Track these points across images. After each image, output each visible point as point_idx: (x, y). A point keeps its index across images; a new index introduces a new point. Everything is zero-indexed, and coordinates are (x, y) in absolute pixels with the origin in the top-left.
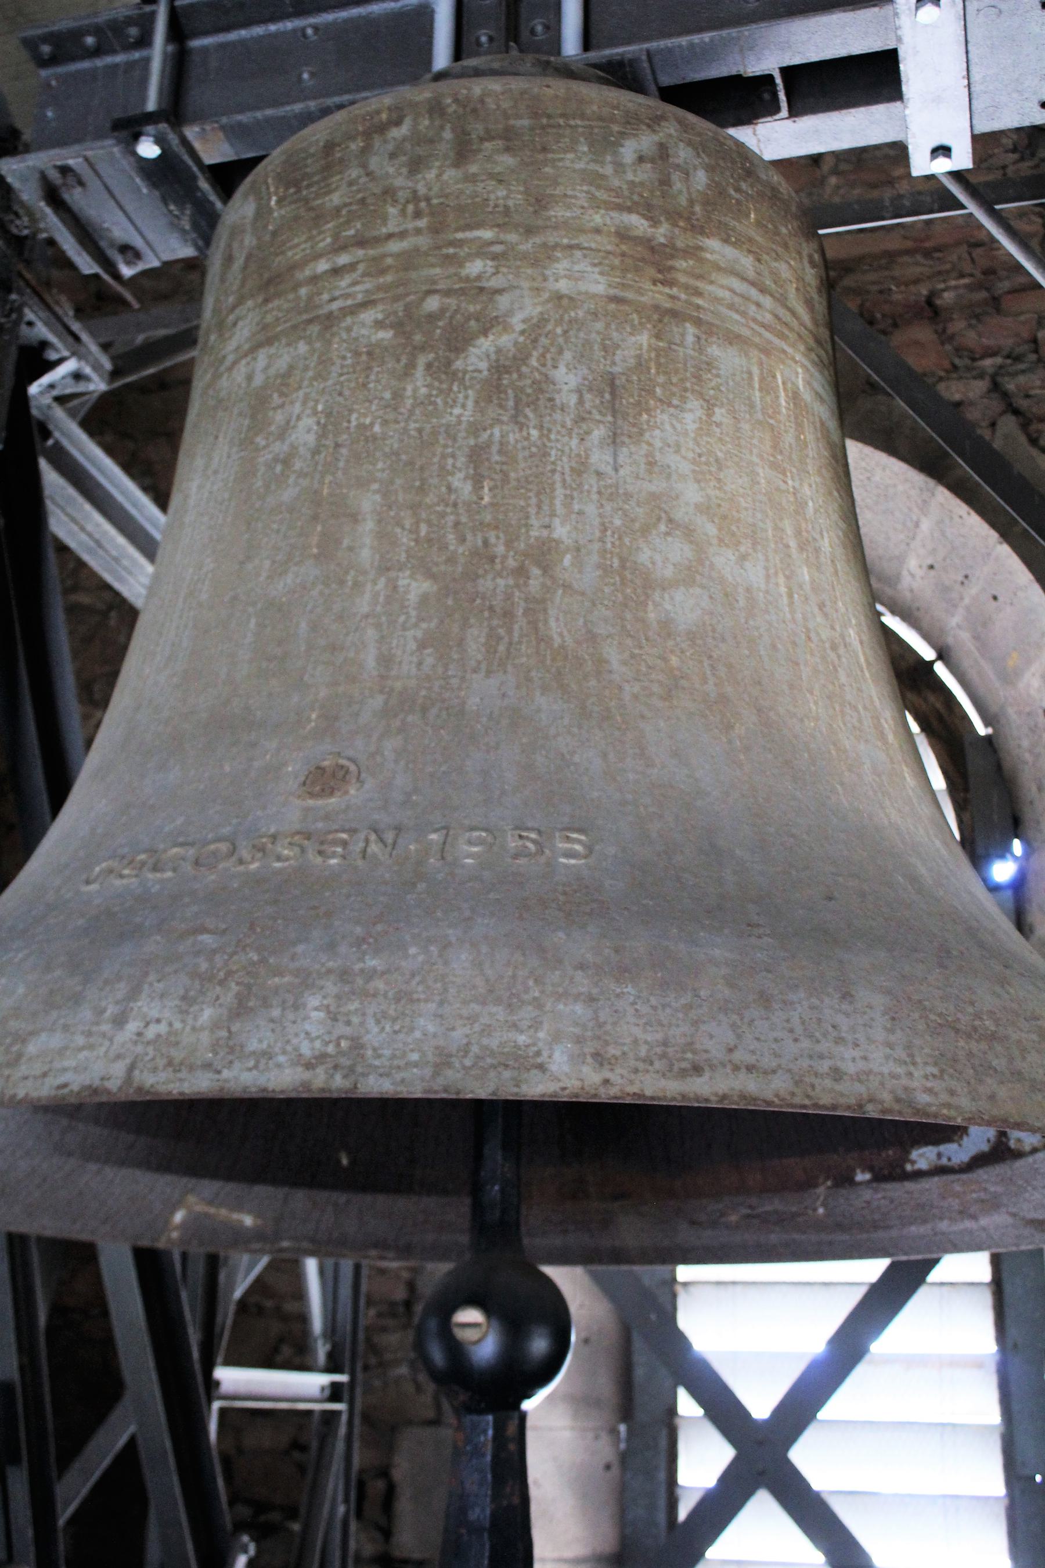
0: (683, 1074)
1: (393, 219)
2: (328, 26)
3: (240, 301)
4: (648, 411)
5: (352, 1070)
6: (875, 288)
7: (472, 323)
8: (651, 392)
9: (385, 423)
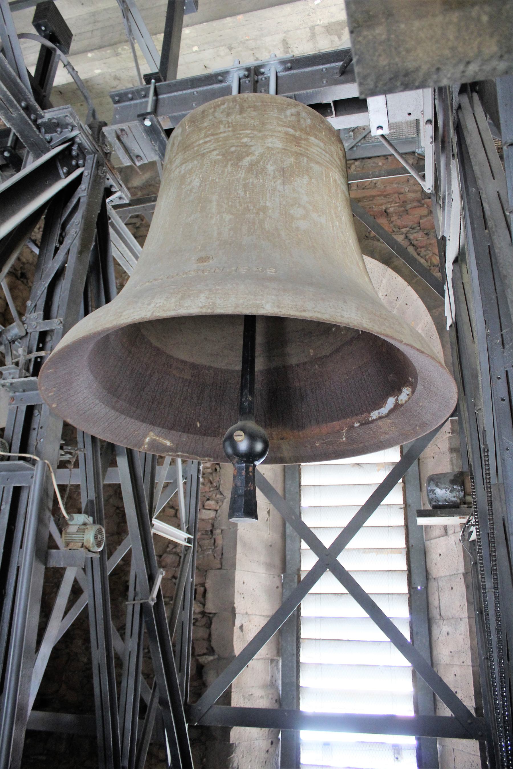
0: (301, 311)
1: (222, 128)
2: (201, 91)
3: (177, 154)
4: (293, 177)
5: (213, 308)
6: (368, 207)
7: (244, 153)
8: (294, 173)
9: (219, 178)
